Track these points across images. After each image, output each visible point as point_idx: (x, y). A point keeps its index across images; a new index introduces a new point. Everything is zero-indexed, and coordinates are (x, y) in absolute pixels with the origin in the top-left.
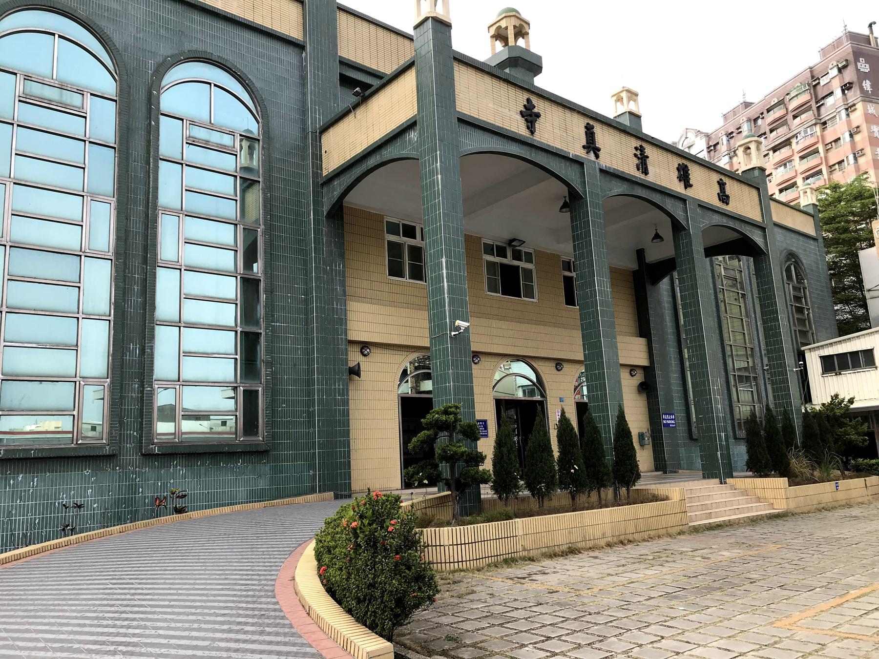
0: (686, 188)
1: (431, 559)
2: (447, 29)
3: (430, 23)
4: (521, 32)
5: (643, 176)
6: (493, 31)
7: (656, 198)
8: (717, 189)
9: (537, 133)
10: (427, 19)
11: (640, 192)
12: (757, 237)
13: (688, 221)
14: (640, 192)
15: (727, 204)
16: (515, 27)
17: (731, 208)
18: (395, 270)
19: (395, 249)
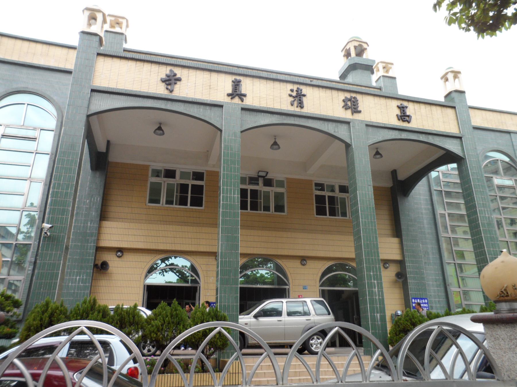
0: (352, 114)
1: (197, 375)
2: (463, 94)
3: (382, 78)
4: (360, 51)
5: (298, 109)
6: (343, 53)
7: (422, 138)
8: (398, 112)
9: (305, 107)
10: (380, 77)
11: (404, 135)
12: (453, 146)
13: (351, 140)
14: (404, 135)
15: (409, 122)
16: (355, 47)
17: (414, 125)
18: (321, 211)
19: (320, 199)
